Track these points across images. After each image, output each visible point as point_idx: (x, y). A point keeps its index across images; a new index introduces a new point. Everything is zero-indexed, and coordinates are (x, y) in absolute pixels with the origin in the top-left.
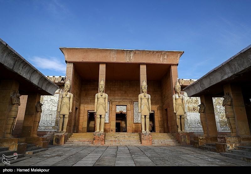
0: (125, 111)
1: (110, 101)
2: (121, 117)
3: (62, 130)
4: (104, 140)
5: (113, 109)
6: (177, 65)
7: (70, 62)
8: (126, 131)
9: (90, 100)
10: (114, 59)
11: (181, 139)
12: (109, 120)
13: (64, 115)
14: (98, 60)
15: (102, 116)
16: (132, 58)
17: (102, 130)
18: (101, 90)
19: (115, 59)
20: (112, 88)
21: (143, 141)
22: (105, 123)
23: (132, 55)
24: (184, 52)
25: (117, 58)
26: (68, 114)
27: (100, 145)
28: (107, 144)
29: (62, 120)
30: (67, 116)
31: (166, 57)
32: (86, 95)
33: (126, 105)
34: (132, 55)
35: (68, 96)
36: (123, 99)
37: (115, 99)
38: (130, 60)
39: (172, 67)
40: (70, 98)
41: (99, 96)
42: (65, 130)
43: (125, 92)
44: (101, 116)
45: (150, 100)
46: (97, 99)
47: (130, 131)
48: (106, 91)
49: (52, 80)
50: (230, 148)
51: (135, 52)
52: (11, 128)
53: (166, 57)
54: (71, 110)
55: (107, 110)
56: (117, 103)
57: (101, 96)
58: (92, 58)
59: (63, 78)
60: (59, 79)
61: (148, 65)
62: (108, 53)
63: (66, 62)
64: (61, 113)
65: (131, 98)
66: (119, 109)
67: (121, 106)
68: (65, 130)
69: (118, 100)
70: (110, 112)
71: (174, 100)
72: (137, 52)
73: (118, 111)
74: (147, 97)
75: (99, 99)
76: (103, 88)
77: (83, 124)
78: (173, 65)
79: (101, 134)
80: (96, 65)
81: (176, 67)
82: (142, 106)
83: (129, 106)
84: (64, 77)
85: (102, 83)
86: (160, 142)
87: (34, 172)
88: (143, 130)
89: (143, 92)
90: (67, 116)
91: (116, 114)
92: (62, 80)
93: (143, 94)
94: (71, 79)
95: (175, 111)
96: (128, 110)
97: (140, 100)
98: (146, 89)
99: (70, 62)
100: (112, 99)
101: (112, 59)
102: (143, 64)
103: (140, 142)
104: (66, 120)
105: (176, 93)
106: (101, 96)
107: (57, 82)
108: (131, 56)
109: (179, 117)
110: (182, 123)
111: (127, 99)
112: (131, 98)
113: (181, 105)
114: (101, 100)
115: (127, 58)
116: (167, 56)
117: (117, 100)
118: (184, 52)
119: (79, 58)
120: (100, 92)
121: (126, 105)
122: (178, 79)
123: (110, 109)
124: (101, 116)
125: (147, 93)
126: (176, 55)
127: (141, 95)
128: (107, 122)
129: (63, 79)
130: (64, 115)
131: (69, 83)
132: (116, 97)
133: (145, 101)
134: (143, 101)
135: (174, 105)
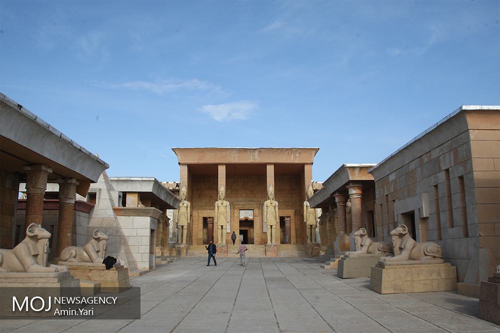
0: (251, 217)
1: (232, 206)
2: (247, 224)
3: (182, 241)
4: (227, 252)
5: (236, 215)
6: (312, 163)
7: (183, 164)
8: (253, 243)
9: (206, 203)
10: (235, 159)
11: (309, 250)
12: (231, 229)
13: (182, 226)
14: (217, 161)
16: (256, 157)
17: (224, 242)
18: (221, 197)
19: (236, 159)
20: (233, 187)
21: (268, 253)
22: (227, 233)
23: (257, 153)
24: (319, 149)
25: (238, 158)
26: (187, 224)
27: (222, 256)
28: (229, 255)
29: (181, 231)
30: (185, 227)
31: (297, 155)
32: (199, 197)
33: (253, 210)
34: (257, 153)
35: (185, 205)
36: (249, 201)
37: (238, 201)
38: (254, 159)
39: (306, 167)
40: (187, 207)
41: (220, 205)
42: (184, 242)
43: (251, 191)
45: (277, 208)
47: (258, 243)
48: (227, 197)
49: (166, 187)
50: (323, 254)
51: (260, 150)
53: (297, 155)
54: (189, 220)
55: (229, 220)
56: (241, 206)
58: (209, 159)
59: (177, 184)
60: (173, 185)
61: (276, 165)
62: (229, 151)
63: (179, 163)
64: (180, 224)
65: (259, 199)
66: (244, 215)
67: (246, 211)
68: (184, 242)
69: (242, 203)
70: (232, 219)
71: (305, 207)
72: (262, 151)
73: (242, 217)
74: (274, 205)
75: (219, 208)
77: (198, 234)
78: (307, 164)
79: (223, 246)
80: (215, 166)
81: (310, 166)
82: (268, 216)
83: (256, 211)
84: (179, 182)
85: (222, 189)
86: (286, 254)
87: (357, 163)
88: (269, 241)
89: (269, 199)
90: (185, 227)
91: (240, 221)
92: (177, 186)
93: (269, 201)
94: (186, 185)
95: (305, 221)
96: (256, 216)
98: (273, 195)
99: (183, 164)
100: (235, 201)
101: (232, 159)
102: (270, 164)
103: (265, 254)
104: (185, 232)
107: (171, 188)
108: (256, 155)
109: (310, 227)
111: (253, 201)
112: (259, 199)
113: (313, 214)
114: (222, 209)
115: (251, 158)
116: (299, 154)
117: (240, 203)
118: (319, 149)
119: (194, 160)
120: (220, 199)
121: (253, 210)
122: (312, 181)
123: (232, 216)
124: (222, 226)
125: (274, 199)
126: (310, 152)
129: (177, 185)
130: (182, 226)
131: (185, 190)
132: (240, 199)
133: (271, 209)
135: (305, 213)
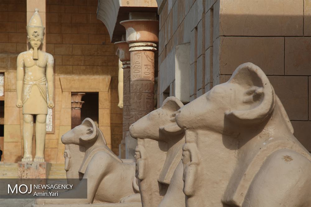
6: (292, 160)
15: (39, 118)
40: (45, 67)
44: (35, 117)
45: (50, 71)
46: (22, 69)
52: (212, 52)
57: (35, 59)
74: (41, 62)
75: (26, 69)
76: (40, 37)
82: (27, 88)
97: (20, 69)
105: (29, 49)
106: (35, 59)
110: (34, 141)
124: (35, 117)
127: (25, 57)
128: (50, 129)
133: (34, 73)
134: (29, 73)
